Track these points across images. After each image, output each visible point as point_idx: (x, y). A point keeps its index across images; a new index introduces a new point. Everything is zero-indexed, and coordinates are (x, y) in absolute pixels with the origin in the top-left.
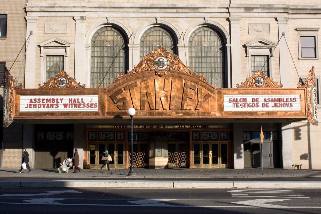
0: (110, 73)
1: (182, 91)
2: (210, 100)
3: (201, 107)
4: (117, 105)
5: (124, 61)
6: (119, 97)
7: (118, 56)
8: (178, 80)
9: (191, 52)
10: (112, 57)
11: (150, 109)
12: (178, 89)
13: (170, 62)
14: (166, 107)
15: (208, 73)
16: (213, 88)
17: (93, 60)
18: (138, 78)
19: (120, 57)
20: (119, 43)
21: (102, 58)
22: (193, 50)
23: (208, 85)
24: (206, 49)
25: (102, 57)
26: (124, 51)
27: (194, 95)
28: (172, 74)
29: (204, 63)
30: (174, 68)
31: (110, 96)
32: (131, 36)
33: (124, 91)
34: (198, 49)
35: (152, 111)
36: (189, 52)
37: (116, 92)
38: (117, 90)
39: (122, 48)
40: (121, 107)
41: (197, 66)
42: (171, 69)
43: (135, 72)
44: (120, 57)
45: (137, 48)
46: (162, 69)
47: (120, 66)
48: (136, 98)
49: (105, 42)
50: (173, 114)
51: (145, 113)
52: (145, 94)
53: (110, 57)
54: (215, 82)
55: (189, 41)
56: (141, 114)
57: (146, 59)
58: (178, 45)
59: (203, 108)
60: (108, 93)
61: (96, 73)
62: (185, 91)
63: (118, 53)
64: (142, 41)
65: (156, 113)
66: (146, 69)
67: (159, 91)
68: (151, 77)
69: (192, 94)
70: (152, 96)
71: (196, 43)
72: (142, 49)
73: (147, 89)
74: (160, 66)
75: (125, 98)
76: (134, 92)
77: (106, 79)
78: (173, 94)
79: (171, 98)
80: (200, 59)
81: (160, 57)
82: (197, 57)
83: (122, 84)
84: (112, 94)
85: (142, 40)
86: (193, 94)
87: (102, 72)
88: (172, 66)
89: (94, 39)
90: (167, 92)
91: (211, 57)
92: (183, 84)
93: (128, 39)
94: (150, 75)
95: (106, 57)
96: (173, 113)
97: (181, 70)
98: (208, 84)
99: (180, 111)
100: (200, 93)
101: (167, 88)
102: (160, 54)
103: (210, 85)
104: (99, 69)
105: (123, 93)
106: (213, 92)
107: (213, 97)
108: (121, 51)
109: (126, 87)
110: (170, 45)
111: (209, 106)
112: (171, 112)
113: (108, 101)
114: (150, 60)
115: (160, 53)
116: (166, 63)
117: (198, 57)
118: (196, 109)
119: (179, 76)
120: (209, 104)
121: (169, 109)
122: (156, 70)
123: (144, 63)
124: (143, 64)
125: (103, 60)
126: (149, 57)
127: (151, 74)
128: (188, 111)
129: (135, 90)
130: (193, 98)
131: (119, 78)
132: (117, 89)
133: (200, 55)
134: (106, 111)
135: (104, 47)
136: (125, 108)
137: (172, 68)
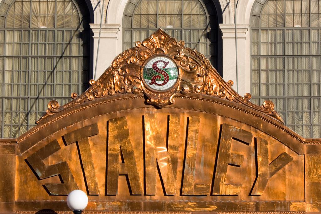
0: (43, 99)
1: (216, 148)
2: (289, 171)
3: (266, 188)
4: (44, 182)
5: (81, 68)
6: (50, 161)
7: (67, 53)
8: (205, 116)
9: (256, 43)
10: (51, 58)
11: (131, 194)
12: (204, 141)
13: (183, 70)
14: (174, 188)
15: (302, 97)
16: (297, 138)
17: (256, 64)
18: (100, 112)
19: (70, 58)
20: (67, 22)
21: (23, 61)
22: (263, 37)
23: (283, 132)
24: (297, 35)
25: (25, 58)
26: (81, 42)
27: (245, 157)
28: (188, 102)
29: (291, 73)
30: (193, 85)
31: (26, 160)
32: (228, 4)
33: (63, 147)
34: (275, 35)
35: (135, 200)
36: (252, 43)
37: (42, 149)
38: (46, 144)
39: (77, 33)
40: (55, 189)
41: (272, 80)
42: (187, 89)
43: (91, 97)
44: (70, 58)
45: (114, 35)
46: (163, 88)
47: (70, 81)
48: (95, 165)
49: (33, 19)
50: (190, 207)
51: (118, 203)
52: (117, 155)
53: (44, 58)
54: (293, 122)
55: (252, 15)
56: (106, 208)
57: (121, 64)
58: (221, 26)
59: (270, 191)
60: (22, 150)
61: (8, 98)
62: (223, 147)
63: (66, 48)
64: (127, 16)
65: (145, 203)
66: (121, 89)
67: (153, 146)
68: (135, 111)
69: (242, 153)
70: (136, 160)
71: (271, 19)
72: (128, 35)
73: (124, 141)
74: (157, 82)
75: (64, 164)
76: (89, 150)
77: (33, 114)
78: (190, 153)
79: (186, 165)
80: (280, 62)
81: (159, 58)
82: (271, 57)
83: (59, 130)
84: (31, 153)
85: (129, 11)
86: (243, 153)
87: (22, 95)
88: (188, 80)
89: (257, 10)
90: (175, 148)
91: (310, 56)
92: (216, 129)
93: (93, 11)
94: (130, 104)
95: (34, 57)
96: (190, 204)
97: (212, 92)
98: (283, 129)
99: (209, 199)
100: (262, 151)
101: (177, 139)
102: (159, 50)
103: (290, 129)
104: (15, 88)
105: (59, 153)
106: (297, 149)
107: (297, 162)
108: (75, 40)
109: (68, 135)
110: (202, 26)
111: (285, 185)
112: (186, 203)
113: (21, 171)
114: (132, 66)
115: (158, 46)
116: (173, 73)
117: (275, 56)
118: (250, 195)
119: (208, 106)
120: (287, 180)
121: (179, 193)
122: (146, 91)
123: (116, 73)
124: (113, 76)
125: (27, 65)
126: (129, 58)
127: (135, 103)
128: (230, 200)
129: (91, 144)
130: (244, 164)
131: (52, 112)
132: (44, 142)
133: (280, 52)
134: (16, 198)
135: (29, 31)
136: (65, 190)
137: (190, 86)
